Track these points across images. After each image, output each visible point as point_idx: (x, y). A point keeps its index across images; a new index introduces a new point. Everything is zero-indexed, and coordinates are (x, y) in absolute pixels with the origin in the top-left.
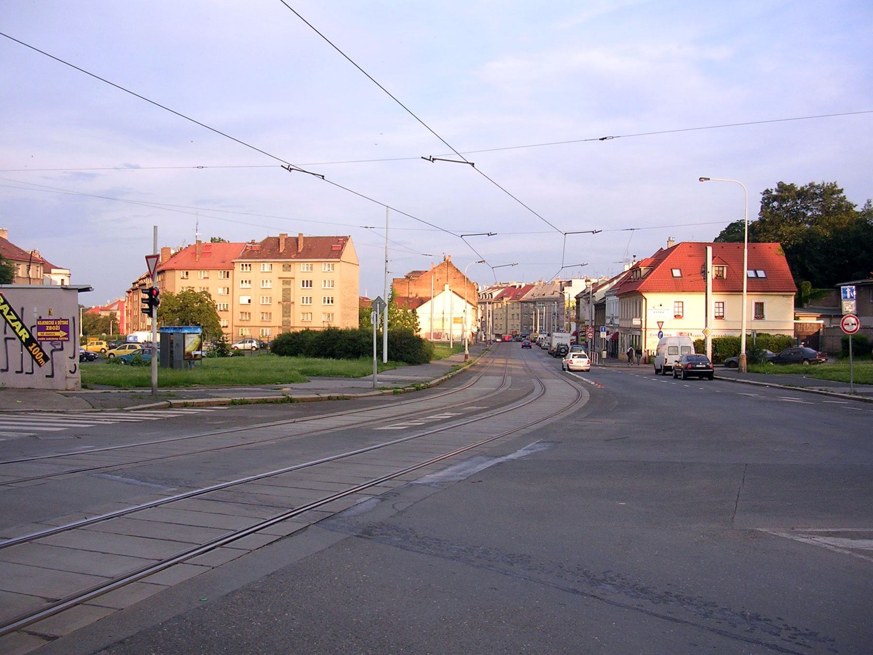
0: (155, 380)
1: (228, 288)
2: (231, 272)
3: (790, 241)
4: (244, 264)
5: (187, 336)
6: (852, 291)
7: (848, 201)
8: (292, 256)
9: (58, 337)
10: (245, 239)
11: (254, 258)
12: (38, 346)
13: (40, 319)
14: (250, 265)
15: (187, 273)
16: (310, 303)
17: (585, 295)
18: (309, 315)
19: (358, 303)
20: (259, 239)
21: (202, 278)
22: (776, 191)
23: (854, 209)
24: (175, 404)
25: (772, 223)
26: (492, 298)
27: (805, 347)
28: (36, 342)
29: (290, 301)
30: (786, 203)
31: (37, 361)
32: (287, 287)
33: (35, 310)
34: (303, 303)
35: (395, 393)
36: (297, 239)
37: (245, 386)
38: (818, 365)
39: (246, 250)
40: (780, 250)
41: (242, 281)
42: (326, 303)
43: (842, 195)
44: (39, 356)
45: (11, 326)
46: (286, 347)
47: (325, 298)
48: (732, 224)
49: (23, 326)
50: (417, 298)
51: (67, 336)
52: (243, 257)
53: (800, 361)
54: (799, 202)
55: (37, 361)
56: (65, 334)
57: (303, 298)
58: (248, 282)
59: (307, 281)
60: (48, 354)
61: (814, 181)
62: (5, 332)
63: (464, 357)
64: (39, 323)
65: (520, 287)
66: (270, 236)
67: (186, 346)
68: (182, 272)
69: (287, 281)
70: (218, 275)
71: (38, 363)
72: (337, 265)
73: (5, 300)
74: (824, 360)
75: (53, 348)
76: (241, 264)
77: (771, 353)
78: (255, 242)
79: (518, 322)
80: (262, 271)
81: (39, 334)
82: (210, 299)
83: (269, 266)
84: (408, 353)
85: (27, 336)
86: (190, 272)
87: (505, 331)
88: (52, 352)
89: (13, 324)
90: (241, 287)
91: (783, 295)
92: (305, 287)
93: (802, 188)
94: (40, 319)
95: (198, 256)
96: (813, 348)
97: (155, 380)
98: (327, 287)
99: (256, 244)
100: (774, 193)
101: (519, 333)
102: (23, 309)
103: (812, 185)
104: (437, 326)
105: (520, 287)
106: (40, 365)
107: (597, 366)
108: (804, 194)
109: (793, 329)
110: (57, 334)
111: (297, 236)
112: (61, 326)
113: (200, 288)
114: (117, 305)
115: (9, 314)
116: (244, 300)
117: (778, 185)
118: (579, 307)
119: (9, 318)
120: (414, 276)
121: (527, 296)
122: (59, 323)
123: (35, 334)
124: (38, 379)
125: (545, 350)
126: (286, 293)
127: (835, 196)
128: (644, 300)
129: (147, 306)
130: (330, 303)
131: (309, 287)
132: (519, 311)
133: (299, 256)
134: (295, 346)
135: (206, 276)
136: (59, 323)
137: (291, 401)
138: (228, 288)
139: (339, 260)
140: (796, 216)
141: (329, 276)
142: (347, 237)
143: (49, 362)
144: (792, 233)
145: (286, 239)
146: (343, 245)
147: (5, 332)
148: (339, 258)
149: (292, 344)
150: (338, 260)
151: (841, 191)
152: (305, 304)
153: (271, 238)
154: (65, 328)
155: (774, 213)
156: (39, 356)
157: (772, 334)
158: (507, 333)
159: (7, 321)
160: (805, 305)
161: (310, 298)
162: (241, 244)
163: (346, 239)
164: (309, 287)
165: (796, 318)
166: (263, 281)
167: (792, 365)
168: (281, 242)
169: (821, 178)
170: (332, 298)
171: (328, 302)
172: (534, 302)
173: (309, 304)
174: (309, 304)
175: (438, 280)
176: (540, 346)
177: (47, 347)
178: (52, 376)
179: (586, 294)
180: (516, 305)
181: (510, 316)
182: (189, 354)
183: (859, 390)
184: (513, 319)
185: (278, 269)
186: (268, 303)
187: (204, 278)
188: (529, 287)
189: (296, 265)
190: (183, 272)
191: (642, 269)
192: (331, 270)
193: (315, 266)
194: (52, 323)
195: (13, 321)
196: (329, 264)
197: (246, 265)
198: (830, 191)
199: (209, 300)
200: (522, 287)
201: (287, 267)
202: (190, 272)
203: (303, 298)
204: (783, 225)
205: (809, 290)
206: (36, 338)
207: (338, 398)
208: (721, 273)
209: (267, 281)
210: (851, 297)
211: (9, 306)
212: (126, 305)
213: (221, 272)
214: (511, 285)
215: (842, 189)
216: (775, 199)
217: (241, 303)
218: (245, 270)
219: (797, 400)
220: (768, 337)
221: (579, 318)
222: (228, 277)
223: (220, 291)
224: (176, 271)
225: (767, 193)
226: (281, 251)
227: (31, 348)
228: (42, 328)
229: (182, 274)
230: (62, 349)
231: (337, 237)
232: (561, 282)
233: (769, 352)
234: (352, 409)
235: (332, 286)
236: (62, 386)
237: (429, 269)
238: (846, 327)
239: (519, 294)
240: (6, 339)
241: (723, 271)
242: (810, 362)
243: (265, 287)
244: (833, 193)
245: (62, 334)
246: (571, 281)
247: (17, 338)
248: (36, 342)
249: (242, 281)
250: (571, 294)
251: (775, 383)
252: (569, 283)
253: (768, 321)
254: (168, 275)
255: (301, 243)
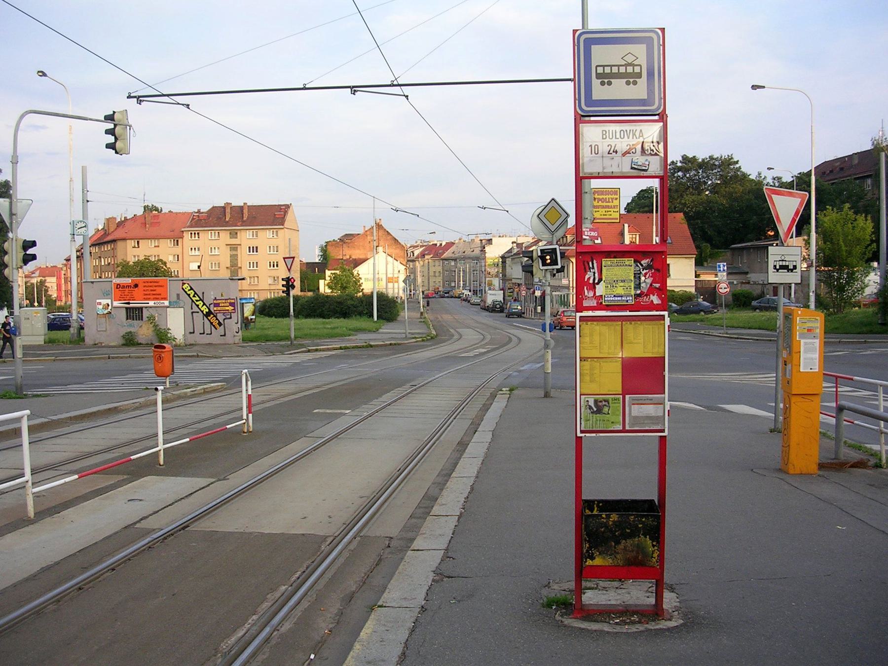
0: (293, 336)
1: (178, 256)
2: (180, 240)
3: (692, 208)
4: (196, 232)
5: (245, 305)
6: (724, 266)
7: (743, 171)
8: (239, 224)
9: (228, 310)
10: (192, 209)
11: (202, 227)
12: (214, 316)
13: (215, 299)
14: (198, 233)
15: (138, 242)
16: (257, 267)
17: (512, 256)
18: (256, 278)
19: (299, 266)
20: (205, 208)
21: (153, 246)
22: (681, 162)
23: (750, 177)
24: (312, 350)
25: (677, 191)
26: (413, 256)
27: (704, 301)
28: (213, 314)
29: (237, 266)
30: (689, 173)
31: (214, 326)
32: (234, 253)
33: (212, 293)
34: (250, 267)
35: (423, 341)
36: (241, 208)
37: (326, 339)
38: (710, 315)
39: (193, 219)
40: (683, 220)
41: (191, 249)
42: (272, 268)
43: (737, 166)
44: (216, 323)
45: (195, 304)
46: (275, 310)
47: (270, 262)
48: (642, 191)
49: (204, 304)
50: (351, 259)
51: (234, 309)
52: (191, 226)
53: (697, 312)
54: (701, 172)
55: (214, 326)
56: (233, 308)
57: (250, 263)
58: (197, 249)
59: (253, 247)
60: (221, 321)
61: (713, 154)
62: (192, 308)
63: (419, 314)
64: (215, 302)
65: (441, 245)
66: (215, 205)
67: (245, 312)
68: (133, 241)
69: (234, 248)
70: (169, 243)
71: (215, 327)
72: (280, 232)
73: (191, 287)
74: (715, 311)
75: (225, 317)
76: (190, 232)
77: (676, 306)
78: (201, 211)
79: (440, 279)
80: (210, 238)
81: (215, 309)
82: (166, 266)
83: (217, 234)
84: (386, 312)
85: (207, 310)
86: (140, 241)
87: (427, 288)
88: (224, 320)
89: (197, 303)
90: (190, 254)
91: (686, 258)
92: (251, 253)
93: (703, 160)
94: (215, 299)
95: (147, 225)
96: (708, 302)
97: (293, 336)
98: (272, 252)
99: (203, 213)
100: (679, 164)
101: (441, 289)
102: (203, 293)
103: (711, 158)
104: (381, 286)
105: (441, 245)
106: (216, 329)
107: (533, 319)
108: (707, 165)
109: (694, 285)
110: (227, 308)
111: (242, 205)
112: (230, 303)
113: (134, 256)
114: (38, 272)
115: (194, 296)
116: (194, 266)
117: (682, 157)
118: (505, 266)
119: (194, 299)
120: (347, 239)
121: (448, 254)
122: (229, 301)
123: (212, 309)
124: (215, 337)
125: (477, 306)
126: (234, 259)
127: (732, 167)
128: (571, 264)
129: (285, 289)
130: (276, 267)
131: (255, 253)
132: (440, 269)
133: (244, 223)
134: (281, 309)
135: (156, 245)
136: (229, 301)
137: (371, 346)
138: (178, 256)
139: (282, 227)
140: (697, 186)
141: (274, 242)
142: (288, 205)
143: (222, 326)
144: (694, 201)
145: (231, 208)
146: (286, 212)
147: (192, 308)
148: (283, 225)
149: (280, 307)
150: (281, 227)
151: (737, 162)
152: (252, 268)
153: (216, 207)
154: (232, 304)
155: (679, 181)
156: (216, 323)
157: (676, 290)
158: (429, 290)
159: (193, 301)
160: (705, 264)
161: (257, 263)
162: (188, 213)
163: (288, 207)
164: (255, 253)
165: (697, 276)
166: (211, 248)
167: (691, 315)
168: (227, 211)
169: (721, 151)
170: (277, 262)
171: (274, 267)
172: (455, 260)
173: (255, 268)
174: (255, 268)
175: (369, 242)
176: (469, 302)
177: (221, 317)
178: (225, 335)
179: (512, 254)
180: (437, 263)
181: (431, 274)
182: (247, 318)
183: (730, 332)
184: (435, 276)
185: (225, 237)
186: (217, 269)
187: (155, 246)
188: (450, 245)
189: (242, 233)
190: (135, 242)
191: (568, 236)
192: (275, 237)
193: (260, 233)
194: (224, 301)
195: (197, 301)
196: (273, 231)
197: (195, 233)
198: (728, 163)
199: (164, 267)
200: (443, 245)
201: (234, 235)
202: (140, 241)
203: (250, 263)
204: (687, 195)
205: (708, 251)
206: (213, 311)
207: (395, 344)
208: (634, 240)
209: (215, 248)
210: (724, 270)
211: (194, 291)
212: (63, 272)
213: (171, 241)
214: (431, 243)
215: (738, 161)
216: (679, 169)
217: (191, 269)
218: (193, 238)
219: (689, 338)
220: (673, 293)
221: (505, 276)
222: (177, 245)
223: (171, 258)
224: (128, 241)
225: (673, 164)
226: (227, 220)
227: (209, 318)
228: (217, 305)
229: (132, 243)
230: (231, 318)
231: (279, 205)
232: (481, 240)
233: (674, 305)
234: (398, 354)
235: (277, 252)
236: (231, 342)
237: (361, 231)
238: (720, 290)
239: (440, 251)
240: (192, 313)
241: (636, 238)
242: (705, 312)
243: (213, 253)
244: (730, 164)
245: (231, 308)
246: (491, 239)
247: (200, 312)
248: (213, 314)
249: (191, 249)
250: (494, 252)
251: (676, 328)
252: (490, 241)
253: (673, 279)
254: (120, 244)
255: (246, 211)
